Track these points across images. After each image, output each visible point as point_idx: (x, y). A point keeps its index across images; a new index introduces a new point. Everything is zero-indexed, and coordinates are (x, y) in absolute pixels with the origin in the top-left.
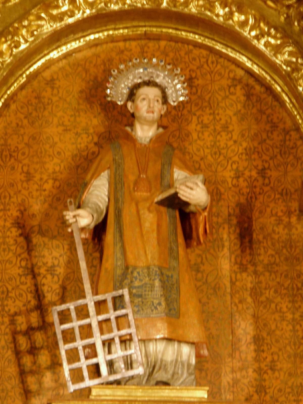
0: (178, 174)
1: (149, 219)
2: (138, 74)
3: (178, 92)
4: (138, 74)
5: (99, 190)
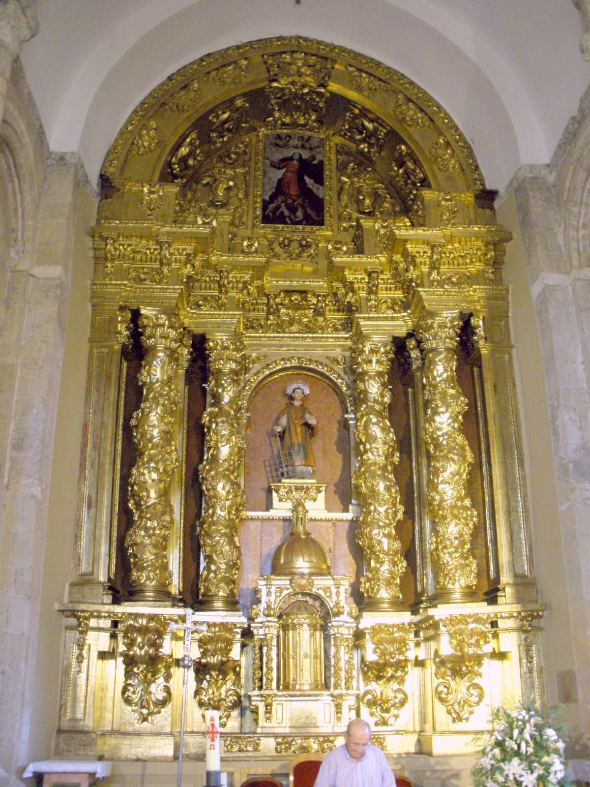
0: (307, 416)
1: (299, 429)
2: (294, 386)
3: (307, 391)
4: (294, 386)
5: (284, 421)
